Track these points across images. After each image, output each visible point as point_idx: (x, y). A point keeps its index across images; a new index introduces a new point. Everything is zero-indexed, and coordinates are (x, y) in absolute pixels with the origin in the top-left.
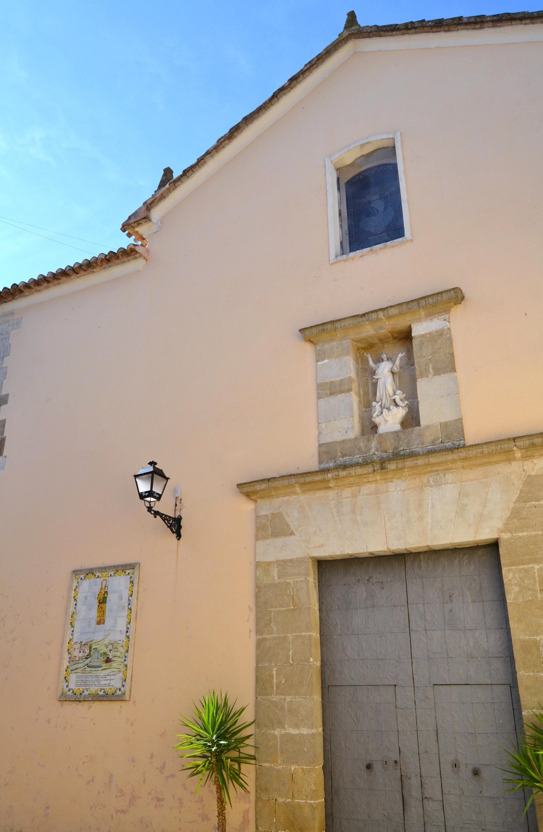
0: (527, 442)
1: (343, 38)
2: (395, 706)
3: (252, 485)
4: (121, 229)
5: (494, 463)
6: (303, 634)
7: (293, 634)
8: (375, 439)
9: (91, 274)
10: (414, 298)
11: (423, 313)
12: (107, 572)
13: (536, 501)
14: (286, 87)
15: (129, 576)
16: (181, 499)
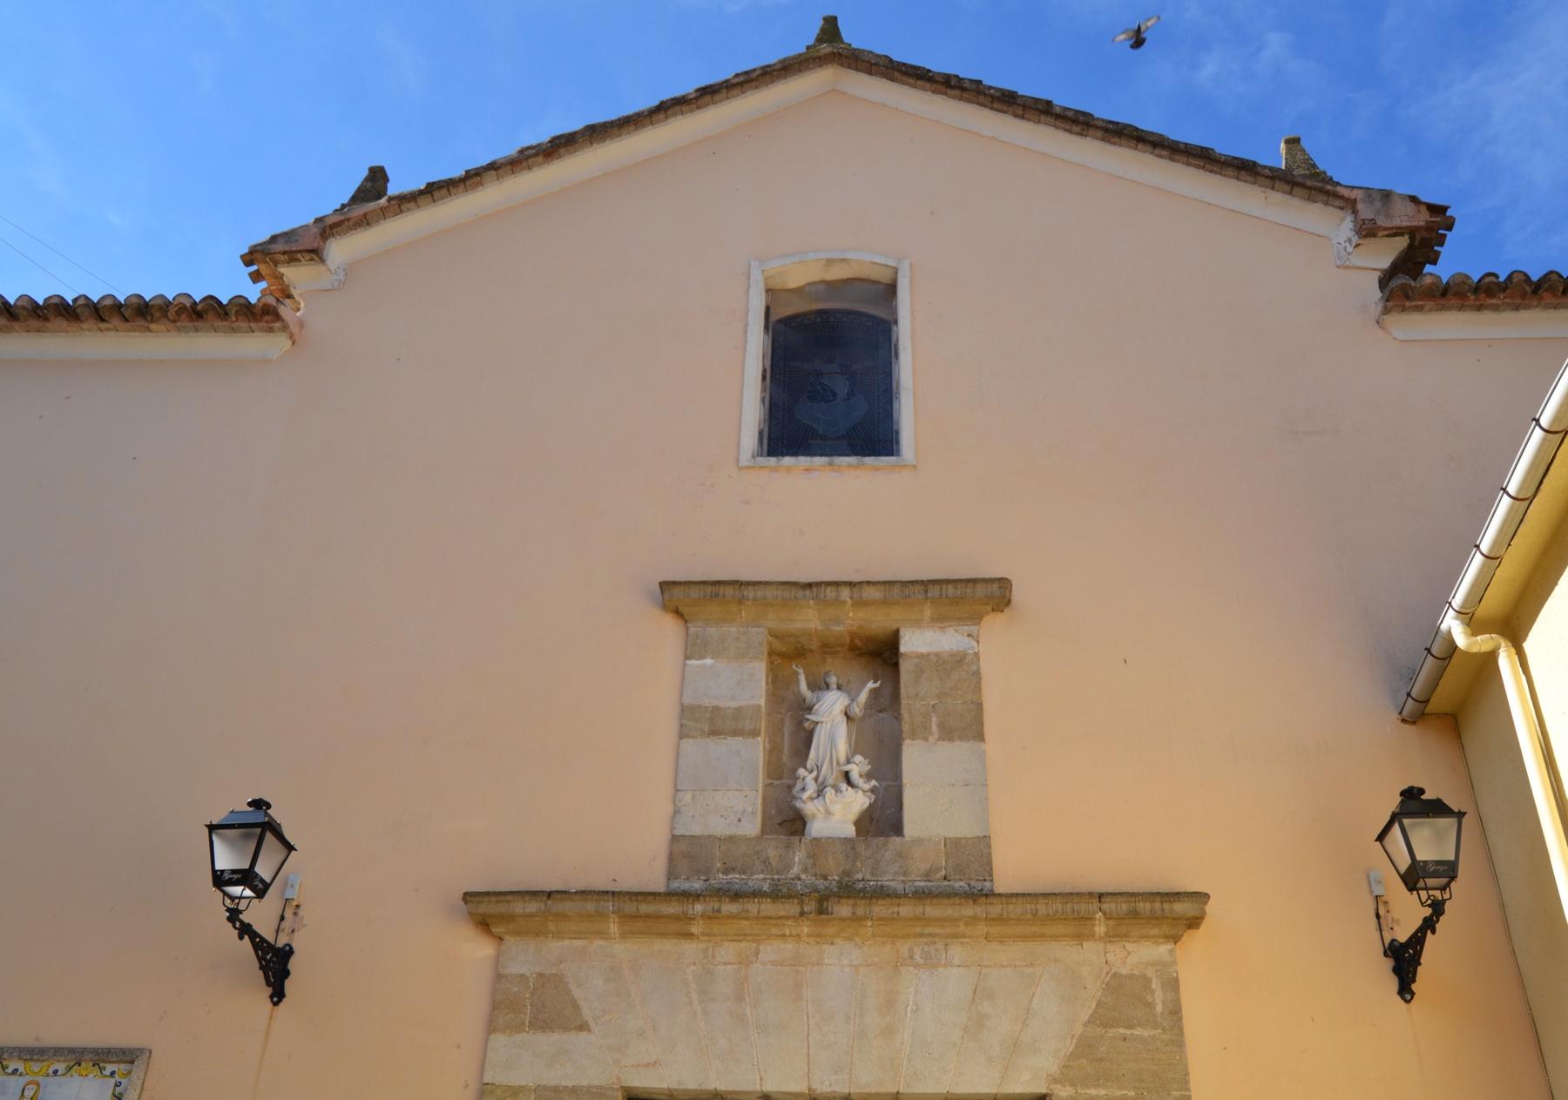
0: (1125, 906)
1: (819, 55)
3: (504, 901)
4: (242, 257)
5: (1049, 939)
8: (803, 847)
9: (139, 332)
10: (919, 578)
11: (929, 612)
12: (45, 1063)
13: (1126, 1028)
14: (690, 100)
15: (112, 1081)
16: (298, 906)
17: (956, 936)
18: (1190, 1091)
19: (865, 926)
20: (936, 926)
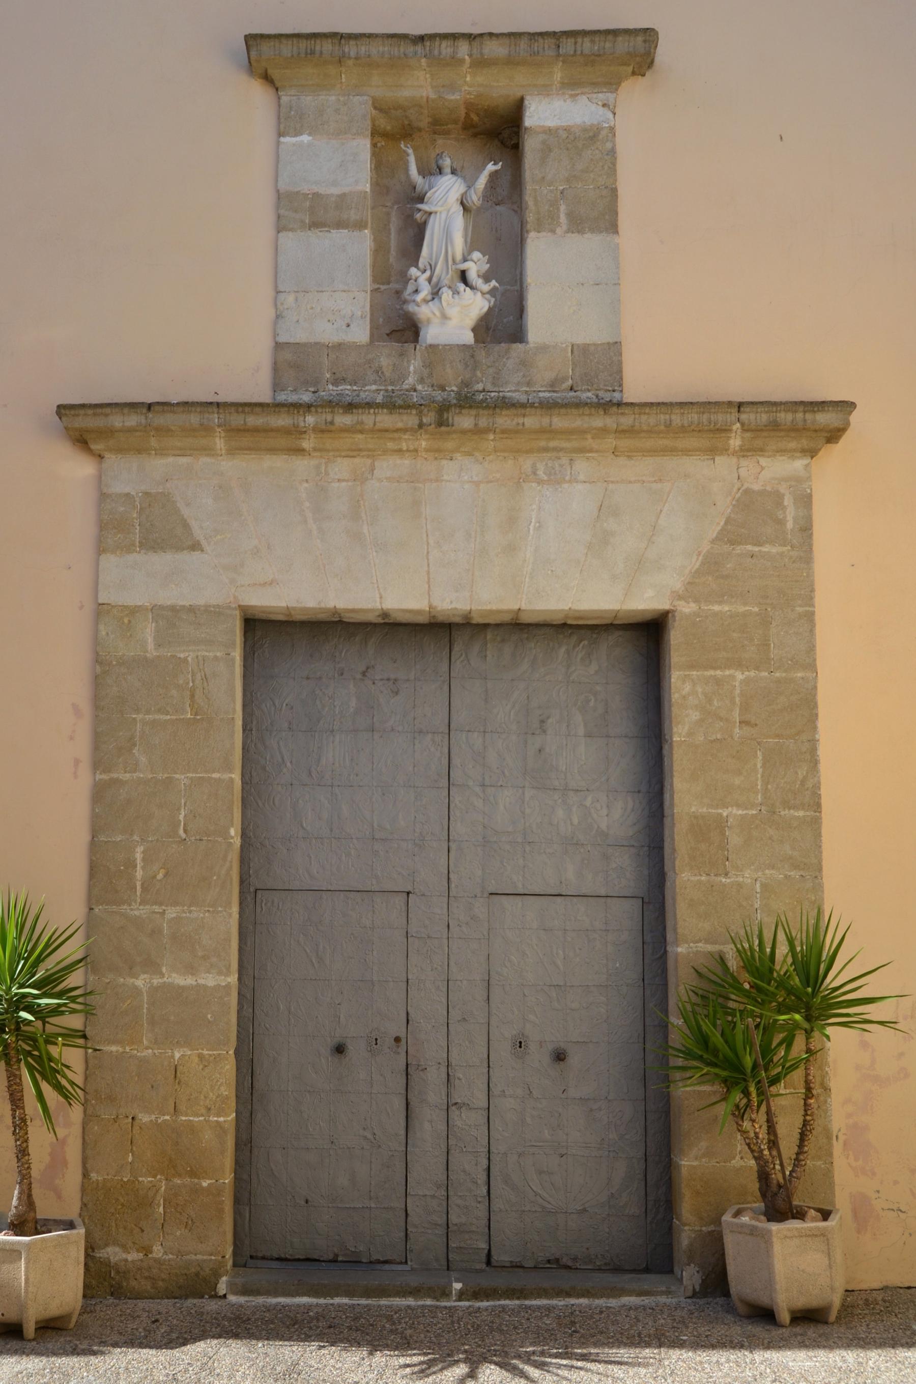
2: (405, 934)
5: (680, 453)
6: (216, 775)
7: (191, 775)
11: (559, 75)
13: (755, 545)
17: (581, 450)
18: (814, 607)
19: (488, 440)
20: (562, 439)
